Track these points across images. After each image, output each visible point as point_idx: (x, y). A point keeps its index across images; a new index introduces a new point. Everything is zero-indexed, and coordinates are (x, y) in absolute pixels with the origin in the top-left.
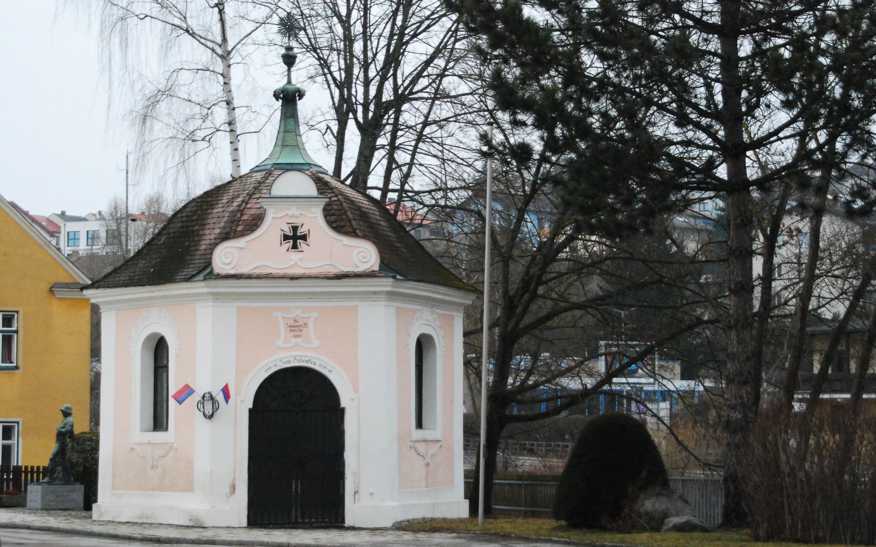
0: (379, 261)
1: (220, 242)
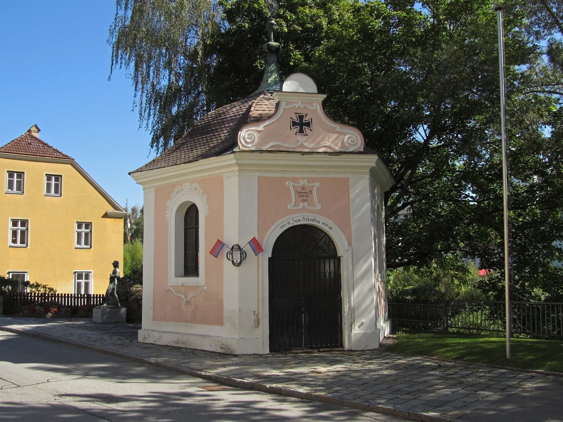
0: (363, 144)
1: (297, 417)
